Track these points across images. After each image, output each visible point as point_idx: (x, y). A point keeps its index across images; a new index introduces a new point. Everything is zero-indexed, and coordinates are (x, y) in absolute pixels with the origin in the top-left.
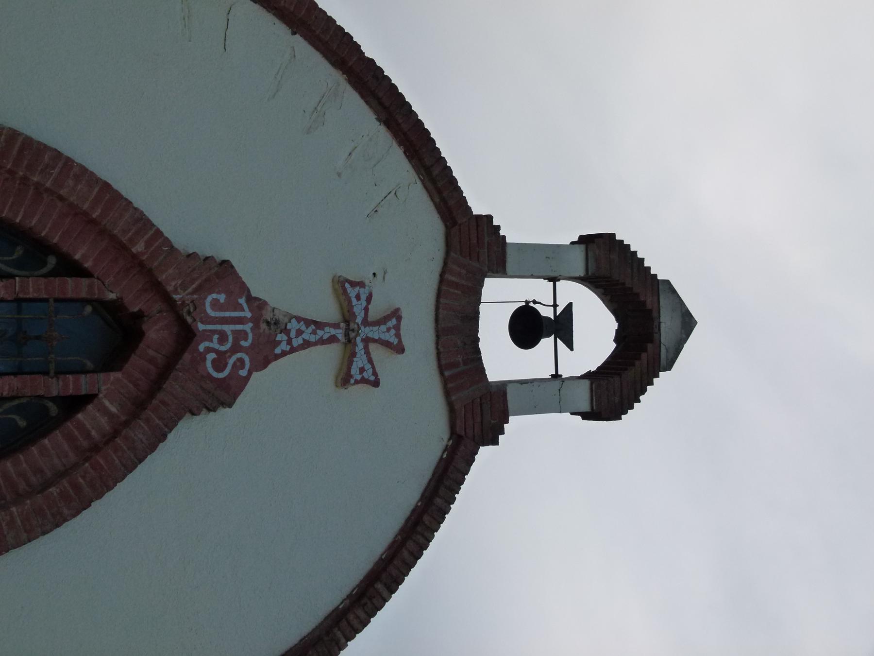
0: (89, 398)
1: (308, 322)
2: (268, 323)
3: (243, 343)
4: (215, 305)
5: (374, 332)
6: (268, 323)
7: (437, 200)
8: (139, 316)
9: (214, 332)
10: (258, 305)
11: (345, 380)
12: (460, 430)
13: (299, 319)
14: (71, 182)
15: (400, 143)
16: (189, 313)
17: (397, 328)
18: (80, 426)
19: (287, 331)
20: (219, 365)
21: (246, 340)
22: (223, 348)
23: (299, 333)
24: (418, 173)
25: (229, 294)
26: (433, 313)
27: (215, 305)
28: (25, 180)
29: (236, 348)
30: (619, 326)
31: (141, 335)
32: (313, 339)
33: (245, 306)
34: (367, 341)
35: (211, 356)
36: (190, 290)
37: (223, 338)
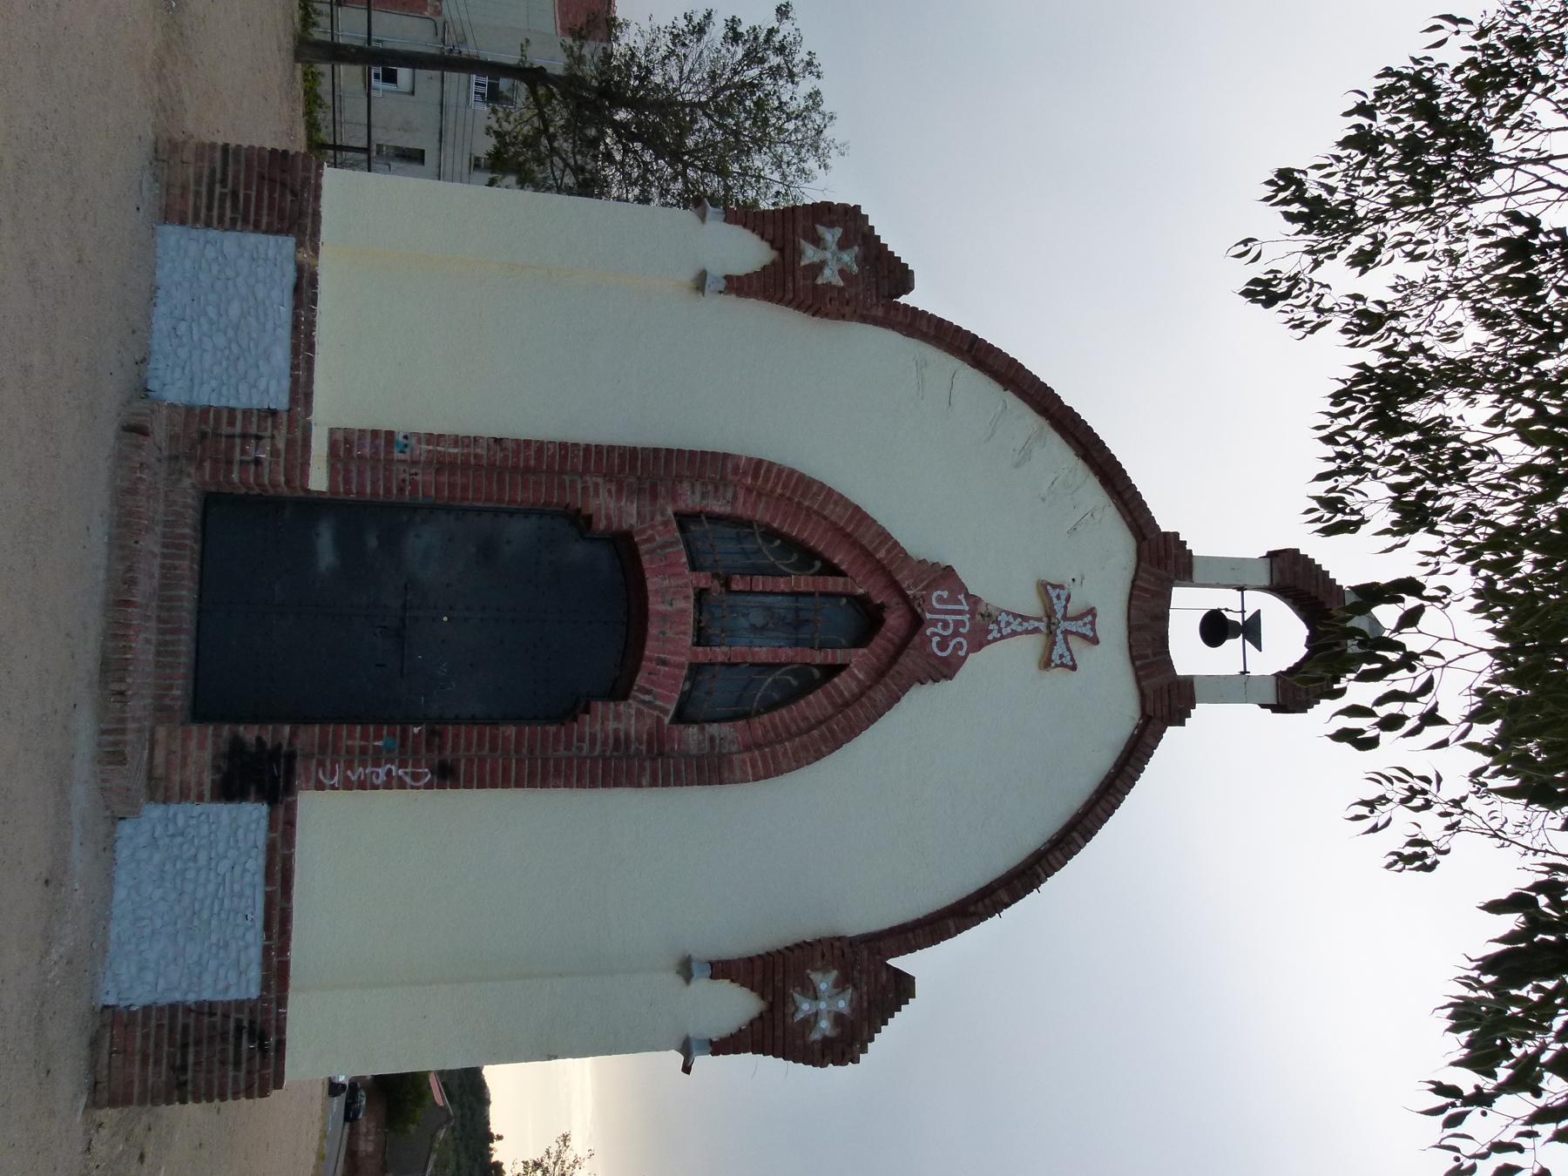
0: (843, 667)
1: (1016, 616)
2: (982, 615)
3: (961, 630)
4: (941, 600)
5: (1072, 626)
6: (982, 615)
7: (1129, 519)
8: (882, 607)
9: (938, 620)
10: (974, 600)
11: (1046, 663)
12: (1149, 711)
13: (1008, 613)
14: (832, 506)
15: (1096, 474)
16: (919, 605)
17: (1093, 623)
18: (836, 687)
19: (998, 623)
20: (943, 645)
21: (964, 627)
22: (945, 633)
23: (1008, 624)
24: (1112, 498)
25: (951, 592)
26: (1126, 615)
27: (941, 600)
28: (799, 504)
29: (956, 634)
30: (1310, 632)
32: (1019, 629)
33: (963, 601)
34: (1066, 633)
35: (936, 639)
36: (920, 587)
37: (946, 625)
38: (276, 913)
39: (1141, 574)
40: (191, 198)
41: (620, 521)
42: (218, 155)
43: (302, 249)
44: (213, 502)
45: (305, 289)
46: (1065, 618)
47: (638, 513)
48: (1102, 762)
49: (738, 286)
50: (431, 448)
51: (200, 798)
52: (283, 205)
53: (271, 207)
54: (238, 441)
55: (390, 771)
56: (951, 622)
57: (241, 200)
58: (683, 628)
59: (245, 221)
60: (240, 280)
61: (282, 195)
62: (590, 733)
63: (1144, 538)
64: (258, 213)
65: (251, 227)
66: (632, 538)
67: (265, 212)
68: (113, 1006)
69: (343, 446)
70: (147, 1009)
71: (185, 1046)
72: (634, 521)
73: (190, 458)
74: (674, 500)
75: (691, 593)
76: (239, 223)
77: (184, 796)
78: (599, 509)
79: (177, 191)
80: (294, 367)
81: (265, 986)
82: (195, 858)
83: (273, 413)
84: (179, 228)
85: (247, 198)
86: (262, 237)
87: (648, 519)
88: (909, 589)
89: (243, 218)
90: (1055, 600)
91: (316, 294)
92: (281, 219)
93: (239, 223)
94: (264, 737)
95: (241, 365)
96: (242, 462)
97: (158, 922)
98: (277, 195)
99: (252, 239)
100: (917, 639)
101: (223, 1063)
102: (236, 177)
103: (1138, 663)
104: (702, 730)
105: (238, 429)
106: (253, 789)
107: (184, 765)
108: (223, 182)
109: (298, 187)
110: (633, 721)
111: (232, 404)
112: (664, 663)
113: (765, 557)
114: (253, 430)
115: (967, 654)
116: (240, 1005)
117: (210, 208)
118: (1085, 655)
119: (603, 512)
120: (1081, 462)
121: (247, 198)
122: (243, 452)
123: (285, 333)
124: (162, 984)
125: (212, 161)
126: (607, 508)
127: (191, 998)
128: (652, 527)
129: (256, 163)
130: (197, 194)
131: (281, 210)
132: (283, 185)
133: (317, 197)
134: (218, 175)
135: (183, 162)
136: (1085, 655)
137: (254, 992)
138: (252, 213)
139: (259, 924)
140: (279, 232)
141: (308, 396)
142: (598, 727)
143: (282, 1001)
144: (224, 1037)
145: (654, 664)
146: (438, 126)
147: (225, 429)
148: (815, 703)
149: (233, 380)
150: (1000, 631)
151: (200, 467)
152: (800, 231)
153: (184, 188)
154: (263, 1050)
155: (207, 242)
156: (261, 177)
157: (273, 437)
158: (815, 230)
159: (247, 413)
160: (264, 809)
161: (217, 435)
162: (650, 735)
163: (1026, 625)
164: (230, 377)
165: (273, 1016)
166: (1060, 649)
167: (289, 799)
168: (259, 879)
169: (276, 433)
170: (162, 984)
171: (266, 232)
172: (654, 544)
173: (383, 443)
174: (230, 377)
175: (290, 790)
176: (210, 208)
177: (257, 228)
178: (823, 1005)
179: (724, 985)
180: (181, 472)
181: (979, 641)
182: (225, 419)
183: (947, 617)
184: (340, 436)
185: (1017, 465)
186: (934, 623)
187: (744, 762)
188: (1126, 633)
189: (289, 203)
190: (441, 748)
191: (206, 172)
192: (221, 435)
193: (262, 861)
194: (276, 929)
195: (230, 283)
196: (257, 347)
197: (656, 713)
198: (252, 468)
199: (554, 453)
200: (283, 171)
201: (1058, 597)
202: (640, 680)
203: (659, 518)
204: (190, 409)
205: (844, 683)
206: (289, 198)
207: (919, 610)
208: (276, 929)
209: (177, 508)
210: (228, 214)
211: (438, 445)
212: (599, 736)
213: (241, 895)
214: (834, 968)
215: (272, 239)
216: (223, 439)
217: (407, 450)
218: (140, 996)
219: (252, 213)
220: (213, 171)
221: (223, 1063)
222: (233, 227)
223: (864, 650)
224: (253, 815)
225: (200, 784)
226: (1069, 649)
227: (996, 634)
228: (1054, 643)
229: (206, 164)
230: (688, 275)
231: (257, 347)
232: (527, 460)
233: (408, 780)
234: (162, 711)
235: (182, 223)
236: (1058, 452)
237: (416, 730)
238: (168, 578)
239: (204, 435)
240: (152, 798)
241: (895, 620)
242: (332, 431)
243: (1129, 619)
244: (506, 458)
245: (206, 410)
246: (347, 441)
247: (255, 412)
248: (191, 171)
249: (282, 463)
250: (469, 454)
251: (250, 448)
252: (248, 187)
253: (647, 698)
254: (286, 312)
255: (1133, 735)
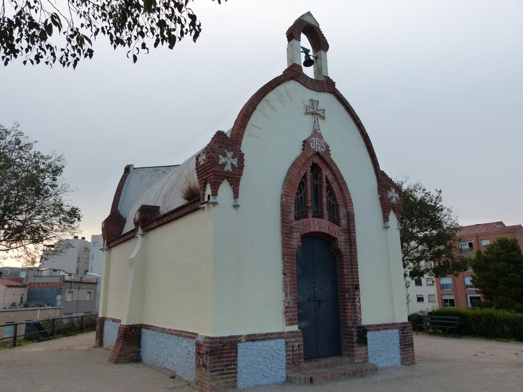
0: (326, 177)
1: (315, 124)
12: (332, 91)
14: (293, 174)
20: (323, 149)
27: (313, 146)
29: (320, 143)
31: (316, 163)
35: (322, 150)
37: (318, 145)
38: (385, 327)
39: (301, 82)
40: (228, 380)
41: (298, 238)
42: (214, 374)
43: (242, 341)
44: (307, 359)
45: (252, 338)
46: (314, 109)
47: (296, 233)
48: (342, 109)
49: (236, 195)
50: (289, 295)
51: (367, 349)
52: (228, 349)
53: (230, 353)
54: (294, 352)
55: (357, 302)
56: (77, 57)
57: (228, 363)
58: (321, 222)
59: (234, 361)
60: (252, 359)
61: (225, 350)
62: (345, 249)
63: (293, 77)
64: (231, 357)
65: (236, 358)
66: (303, 235)
67: (231, 355)
68: (401, 362)
69: (290, 322)
70: (401, 355)
71: (406, 345)
72: (298, 234)
73: (299, 366)
74: (292, 221)
75: (313, 219)
76: (235, 363)
77: (367, 353)
78: (297, 244)
79: (227, 385)
80: (274, 338)
81: (396, 328)
82: (377, 348)
83: (286, 343)
84: (238, 382)
85: (227, 361)
86: (239, 354)
87: (298, 230)
88: (311, 154)
89: (234, 361)
90: (310, 111)
91: (253, 334)
92: (233, 349)
93: (235, 363)
94: (356, 335)
95: (275, 355)
96: (299, 350)
97: (388, 355)
98: (225, 352)
99: (239, 358)
100: (322, 155)
101: (408, 336)
102: (221, 366)
103: (322, 91)
104: (342, 219)
105: (291, 353)
106: (365, 336)
107: (361, 354)
108: (223, 370)
109: (222, 344)
110: (341, 237)
111: (285, 356)
112: (329, 228)
113: (302, 195)
114: (291, 348)
115: (324, 141)
116: (400, 333)
117: (231, 373)
118: (321, 106)
119: (297, 243)
120: (274, 90)
121: (227, 361)
122: (296, 350)
123: (265, 343)
124: (397, 352)
125: (216, 375)
126: (296, 242)
127: (399, 345)
128: (300, 229)
129: (216, 360)
130: (227, 378)
131: (230, 349)
132: (222, 350)
133: (224, 338)
134: (221, 372)
135: (218, 385)
136: (321, 106)
137: (397, 331)
138: (232, 359)
139: (386, 331)
140: (237, 349)
141: (280, 333)
142: (343, 247)
143: (397, 324)
144: (404, 336)
145: (330, 231)
146: (30, 311)
147: (291, 357)
148: (335, 186)
149: (279, 357)
150: (318, 130)
151: (300, 362)
152: (221, 170)
153: (227, 383)
154: (406, 327)
155: (241, 372)
156: (220, 358)
157: (292, 342)
158: (220, 165)
159: (287, 351)
160: (368, 333)
161: (293, 359)
162: (344, 233)
163: (316, 122)
164: (278, 358)
165: (400, 326)
166: (320, 113)
167: (365, 327)
168: (380, 332)
169: (291, 342)
170: (397, 352)
171: (237, 353)
172: (304, 229)
173: (288, 310)
174: (278, 358)
175: (363, 327)
176: (231, 373)
177: (236, 357)
178: (394, 195)
179: (219, 192)
180: (302, 368)
181: (321, 137)
182: (289, 357)
183: (317, 144)
184: (288, 323)
185: (276, 111)
186: (318, 149)
187: (350, 208)
188: (314, 91)
189: (227, 347)
190: (350, 289)
191: (220, 377)
192: (293, 358)
193: (377, 332)
194: (387, 327)
195: (253, 362)
196: (269, 351)
197: (339, 231)
198: (300, 347)
199: (287, 257)
200: (217, 350)
201: (309, 109)
202: (333, 235)
203: (297, 227)
204: (287, 368)
205: (330, 177)
206: (226, 347)
207: (315, 152)
208: (387, 327)
209: (311, 367)
210: (233, 367)
211: (287, 293)
212: (345, 247)
213: (382, 336)
214: (387, 191)
215: (239, 351)
216: (294, 357)
217: (290, 302)
218: (399, 357)
219: (232, 359)
220: (220, 374)
221: (408, 336)
222: (236, 364)
223: (323, 170)
224: (370, 335)
225: (365, 350)
226: (321, 110)
227: (319, 131)
228: (319, 114)
229: (217, 377)
230: (233, 210)
231: (269, 351)
232: (289, 266)
233: (358, 297)
234: (352, 362)
235: (236, 381)
236: (271, 96)
237: (347, 296)
238: (325, 366)
239: (294, 363)
240: (367, 361)
241: (316, 160)
242: (287, 325)
243: (311, 89)
244: (289, 272)
245: (287, 364)
246: (289, 321)
247: (286, 349)
248: (220, 382)
249: (298, 339)
250: (289, 283)
251: (295, 348)
252: (223, 362)
253: (337, 233)
254: (259, 343)
255: (336, 98)
